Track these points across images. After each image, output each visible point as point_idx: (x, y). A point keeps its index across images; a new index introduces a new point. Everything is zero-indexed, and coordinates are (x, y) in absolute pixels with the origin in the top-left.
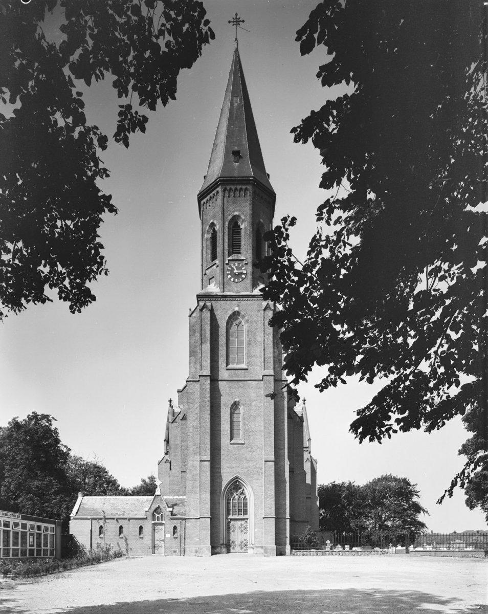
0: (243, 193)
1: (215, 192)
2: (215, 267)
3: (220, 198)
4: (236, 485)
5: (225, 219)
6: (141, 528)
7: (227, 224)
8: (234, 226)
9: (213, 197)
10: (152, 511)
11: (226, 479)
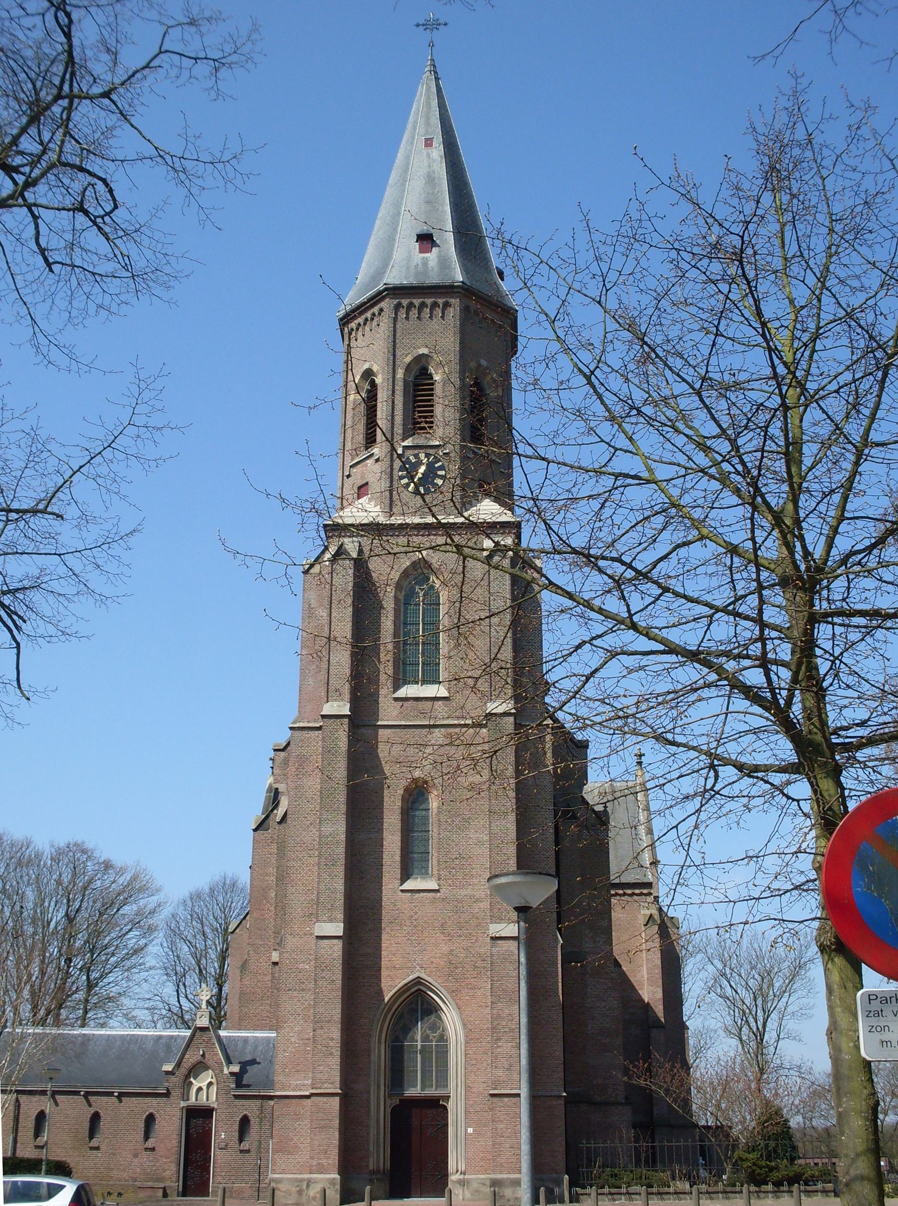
0: (440, 311)
1: (376, 310)
2: (370, 462)
3: (385, 322)
4: (418, 1003)
5: (398, 363)
6: (150, 1120)
7: (400, 374)
8: (419, 384)
9: (372, 319)
10: (183, 1070)
11: (392, 983)
